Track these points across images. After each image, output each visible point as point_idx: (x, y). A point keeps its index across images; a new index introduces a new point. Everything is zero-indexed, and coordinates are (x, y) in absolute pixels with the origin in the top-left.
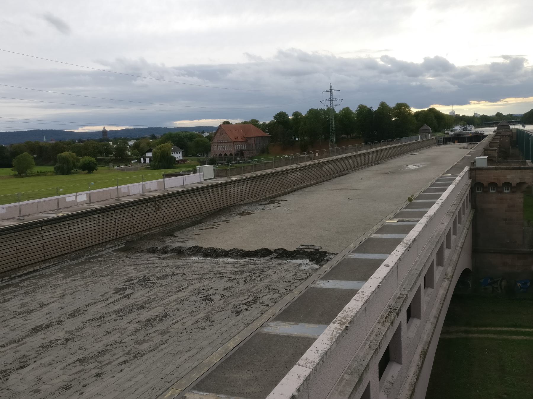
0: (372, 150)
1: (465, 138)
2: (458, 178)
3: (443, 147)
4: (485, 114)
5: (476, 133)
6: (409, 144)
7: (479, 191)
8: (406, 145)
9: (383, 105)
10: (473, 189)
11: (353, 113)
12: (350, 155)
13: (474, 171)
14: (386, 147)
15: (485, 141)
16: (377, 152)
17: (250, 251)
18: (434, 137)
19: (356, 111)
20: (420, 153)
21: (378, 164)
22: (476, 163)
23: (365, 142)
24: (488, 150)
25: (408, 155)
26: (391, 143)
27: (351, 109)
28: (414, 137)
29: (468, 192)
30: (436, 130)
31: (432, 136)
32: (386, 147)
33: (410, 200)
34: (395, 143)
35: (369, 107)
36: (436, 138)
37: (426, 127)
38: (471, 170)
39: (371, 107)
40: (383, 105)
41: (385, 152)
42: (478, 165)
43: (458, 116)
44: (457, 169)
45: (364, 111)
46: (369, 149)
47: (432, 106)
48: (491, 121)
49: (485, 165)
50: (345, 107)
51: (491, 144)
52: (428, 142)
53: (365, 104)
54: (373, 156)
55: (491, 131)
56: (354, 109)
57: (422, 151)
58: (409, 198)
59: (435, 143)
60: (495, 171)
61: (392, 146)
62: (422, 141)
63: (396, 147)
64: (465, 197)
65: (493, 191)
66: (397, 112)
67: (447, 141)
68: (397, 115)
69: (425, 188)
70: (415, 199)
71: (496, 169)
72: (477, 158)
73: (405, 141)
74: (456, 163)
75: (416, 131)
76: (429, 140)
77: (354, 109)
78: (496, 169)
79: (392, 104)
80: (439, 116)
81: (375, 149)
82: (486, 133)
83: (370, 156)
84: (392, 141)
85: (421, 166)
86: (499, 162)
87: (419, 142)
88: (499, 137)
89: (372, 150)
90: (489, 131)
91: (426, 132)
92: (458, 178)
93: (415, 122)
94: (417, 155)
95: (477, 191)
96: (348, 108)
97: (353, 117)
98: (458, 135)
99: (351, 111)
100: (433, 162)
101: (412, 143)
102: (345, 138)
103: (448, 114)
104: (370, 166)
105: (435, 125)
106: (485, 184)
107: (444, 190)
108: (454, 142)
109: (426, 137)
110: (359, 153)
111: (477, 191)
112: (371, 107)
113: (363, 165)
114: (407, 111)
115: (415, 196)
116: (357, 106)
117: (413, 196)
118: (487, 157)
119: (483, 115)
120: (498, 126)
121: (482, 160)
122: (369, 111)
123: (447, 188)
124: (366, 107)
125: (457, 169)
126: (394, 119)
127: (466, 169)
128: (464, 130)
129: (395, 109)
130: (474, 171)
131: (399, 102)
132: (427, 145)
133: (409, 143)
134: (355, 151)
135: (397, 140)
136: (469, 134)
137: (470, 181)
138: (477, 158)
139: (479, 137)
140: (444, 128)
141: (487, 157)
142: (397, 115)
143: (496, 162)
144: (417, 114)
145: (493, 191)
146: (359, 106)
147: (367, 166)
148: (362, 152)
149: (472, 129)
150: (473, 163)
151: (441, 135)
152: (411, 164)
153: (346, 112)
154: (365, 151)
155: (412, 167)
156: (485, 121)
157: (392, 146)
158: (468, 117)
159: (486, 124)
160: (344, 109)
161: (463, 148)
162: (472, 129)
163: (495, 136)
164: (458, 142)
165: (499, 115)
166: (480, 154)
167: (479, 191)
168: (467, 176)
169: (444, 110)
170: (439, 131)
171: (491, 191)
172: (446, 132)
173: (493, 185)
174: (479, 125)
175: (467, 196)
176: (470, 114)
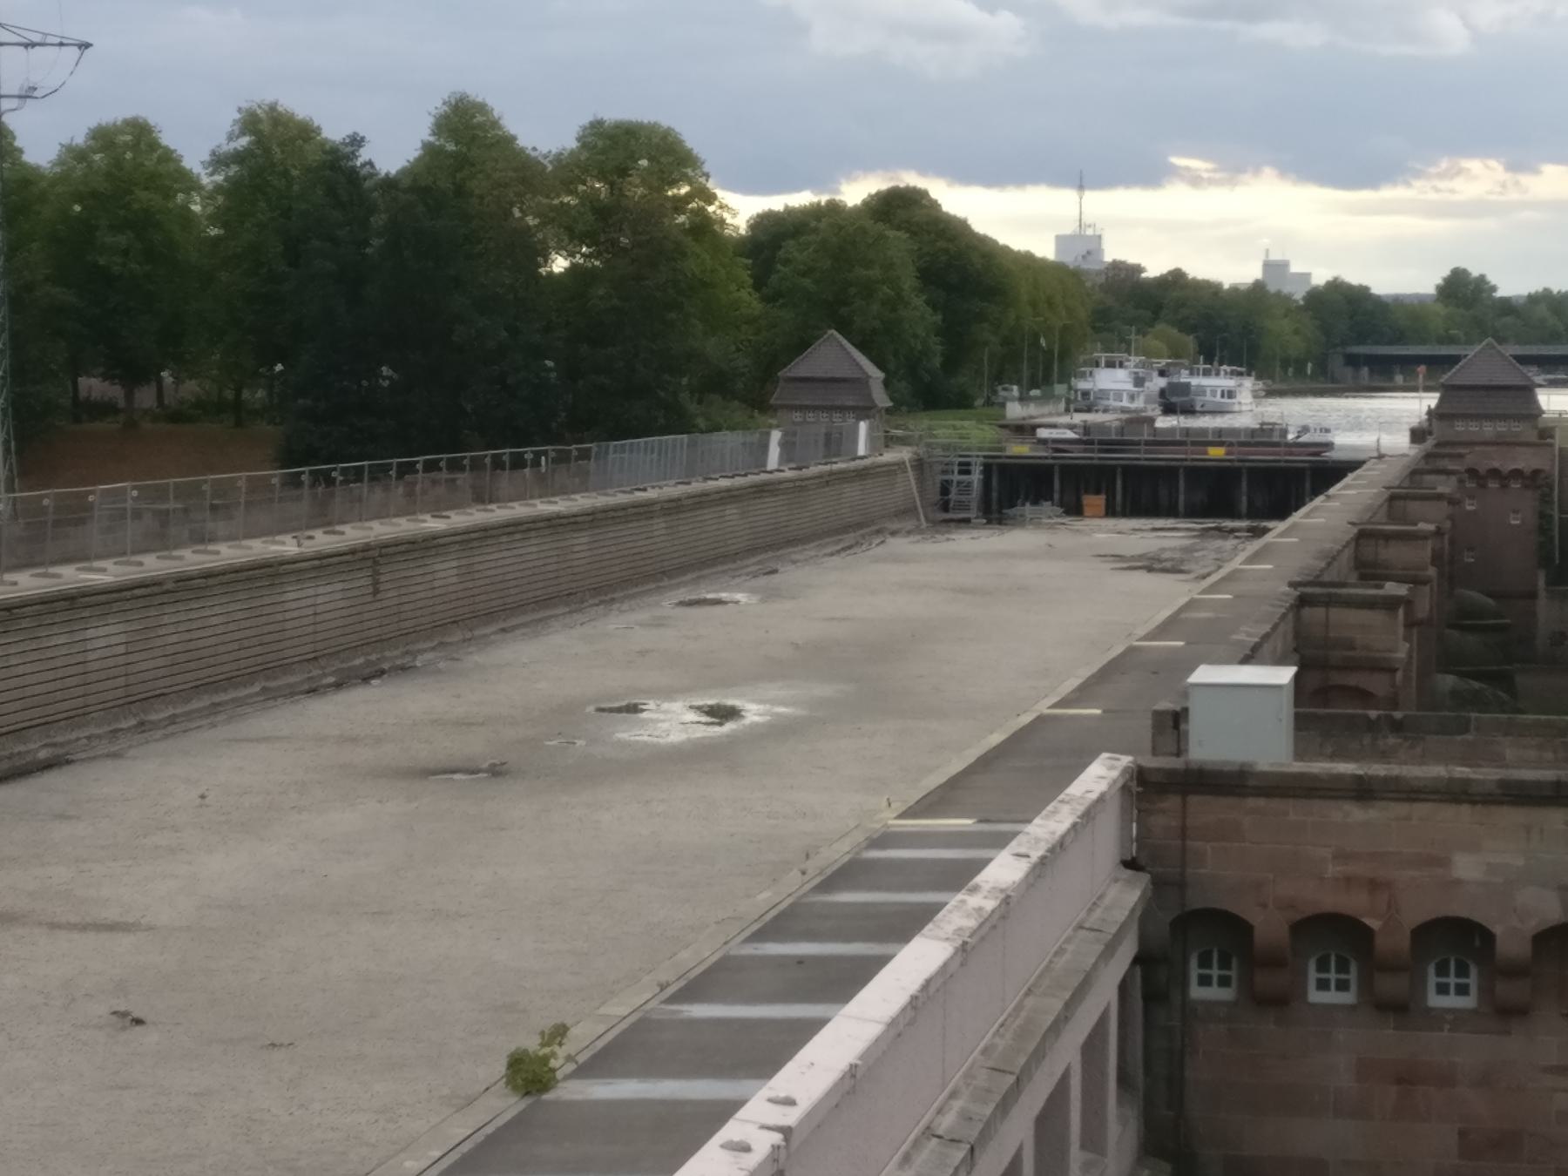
0: (322, 541)
1: (1167, 474)
2: (1004, 870)
3: (979, 546)
4: (1354, 278)
5: (1265, 436)
6: (673, 507)
7: (1214, 993)
8: (644, 511)
9: (466, 132)
10: (1153, 976)
11: (188, 182)
12: (107, 573)
13: (1172, 802)
14: (460, 519)
15: (1325, 519)
16: (371, 557)
17: (928, 984)
18: (903, 454)
19: (218, 161)
20: (769, 595)
21: (366, 677)
22: (1196, 727)
23: (289, 457)
24: (1329, 602)
25: (666, 603)
26: (505, 480)
27: (167, 139)
28: (729, 441)
29: (1105, 994)
30: (927, 390)
31: (890, 442)
32: (460, 519)
33: (529, 1075)
34: (547, 489)
35: (333, 131)
36: (919, 465)
37: (833, 354)
38: (1143, 789)
39: (356, 141)
40: (466, 132)
41: (446, 570)
42: (1209, 745)
43: (1124, 279)
44: (1025, 764)
45: (288, 172)
46: (437, 509)
47: (910, 179)
48: (1400, 338)
49: (1269, 746)
50: (113, 113)
51: (1367, 547)
52: (851, 492)
53: (301, 104)
54: (328, 595)
55: (1385, 425)
56: (198, 139)
57: (789, 575)
58: (517, 1063)
59: (907, 512)
60: (1356, 813)
61: (518, 510)
62: (798, 488)
63: (553, 524)
64: (1067, 1053)
65: (1332, 997)
66: (590, 200)
67: (1019, 488)
68: (597, 225)
69: (699, 954)
70: (588, 1070)
71: (1363, 791)
72: (1205, 674)
73: (642, 477)
74: (1043, 708)
75: (753, 388)
76: (862, 474)
77: (198, 139)
78: (1363, 791)
79: (544, 130)
80: (961, 271)
81: (353, 534)
82: (1346, 441)
83: (297, 598)
84: (518, 463)
85: (754, 713)
86: (1397, 727)
87: (761, 490)
88: (1445, 486)
89: (322, 541)
90: (1379, 424)
91: (842, 396)
92: (1004, 870)
93: (749, 301)
94: (745, 611)
95: (1197, 992)
96: (141, 133)
97: (186, 216)
98: (1109, 445)
99: (168, 156)
100: (866, 679)
101: (701, 501)
102: (104, 409)
103: (1045, 250)
104: (291, 693)
105: (920, 349)
106: (1269, 927)
107: (844, 980)
108: (1074, 509)
109: (836, 444)
110: (191, 559)
111: (1197, 992)
112: (356, 141)
113: (231, 681)
114: (679, 204)
115: (585, 1036)
116: (227, 118)
117: (559, 1033)
118: (1284, 675)
119: (1336, 286)
120: (1448, 391)
121: (1245, 698)
122: (338, 170)
123: (881, 961)
124: (306, 132)
125: (1025, 764)
126: (559, 264)
127: (1099, 776)
128: (1169, 409)
129: (569, 170)
130: (1173, 793)
131: (617, 111)
132: (838, 520)
133: (672, 490)
134: (160, 541)
135: (562, 458)
136: (1201, 440)
137: (1128, 896)
138: (1205, 674)
139: (1281, 480)
140: (999, 378)
141: (1284, 675)
142: (597, 225)
143: (1372, 726)
144: (774, 233)
145: (1332, 997)
146: (249, 122)
147: (271, 696)
148: (227, 554)
149: (1241, 406)
150: (1173, 723)
151: (965, 435)
152: (669, 694)
153: (125, 167)
154: (259, 549)
155: (674, 722)
156: (1347, 336)
157: (518, 510)
158: (1210, 290)
159: (1353, 361)
160: (103, 137)
161: (1151, 564)
162: (1241, 406)
163: (1415, 474)
164: (1111, 512)
165: (1462, 291)
166: (1248, 634)
167: (1214, 993)
168: (1107, 842)
169: (1018, 219)
170: (961, 402)
171: (1315, 996)
172: (1015, 411)
173: (1336, 935)
174: (1300, 371)
175: (1092, 1048)
176: (1233, 270)
